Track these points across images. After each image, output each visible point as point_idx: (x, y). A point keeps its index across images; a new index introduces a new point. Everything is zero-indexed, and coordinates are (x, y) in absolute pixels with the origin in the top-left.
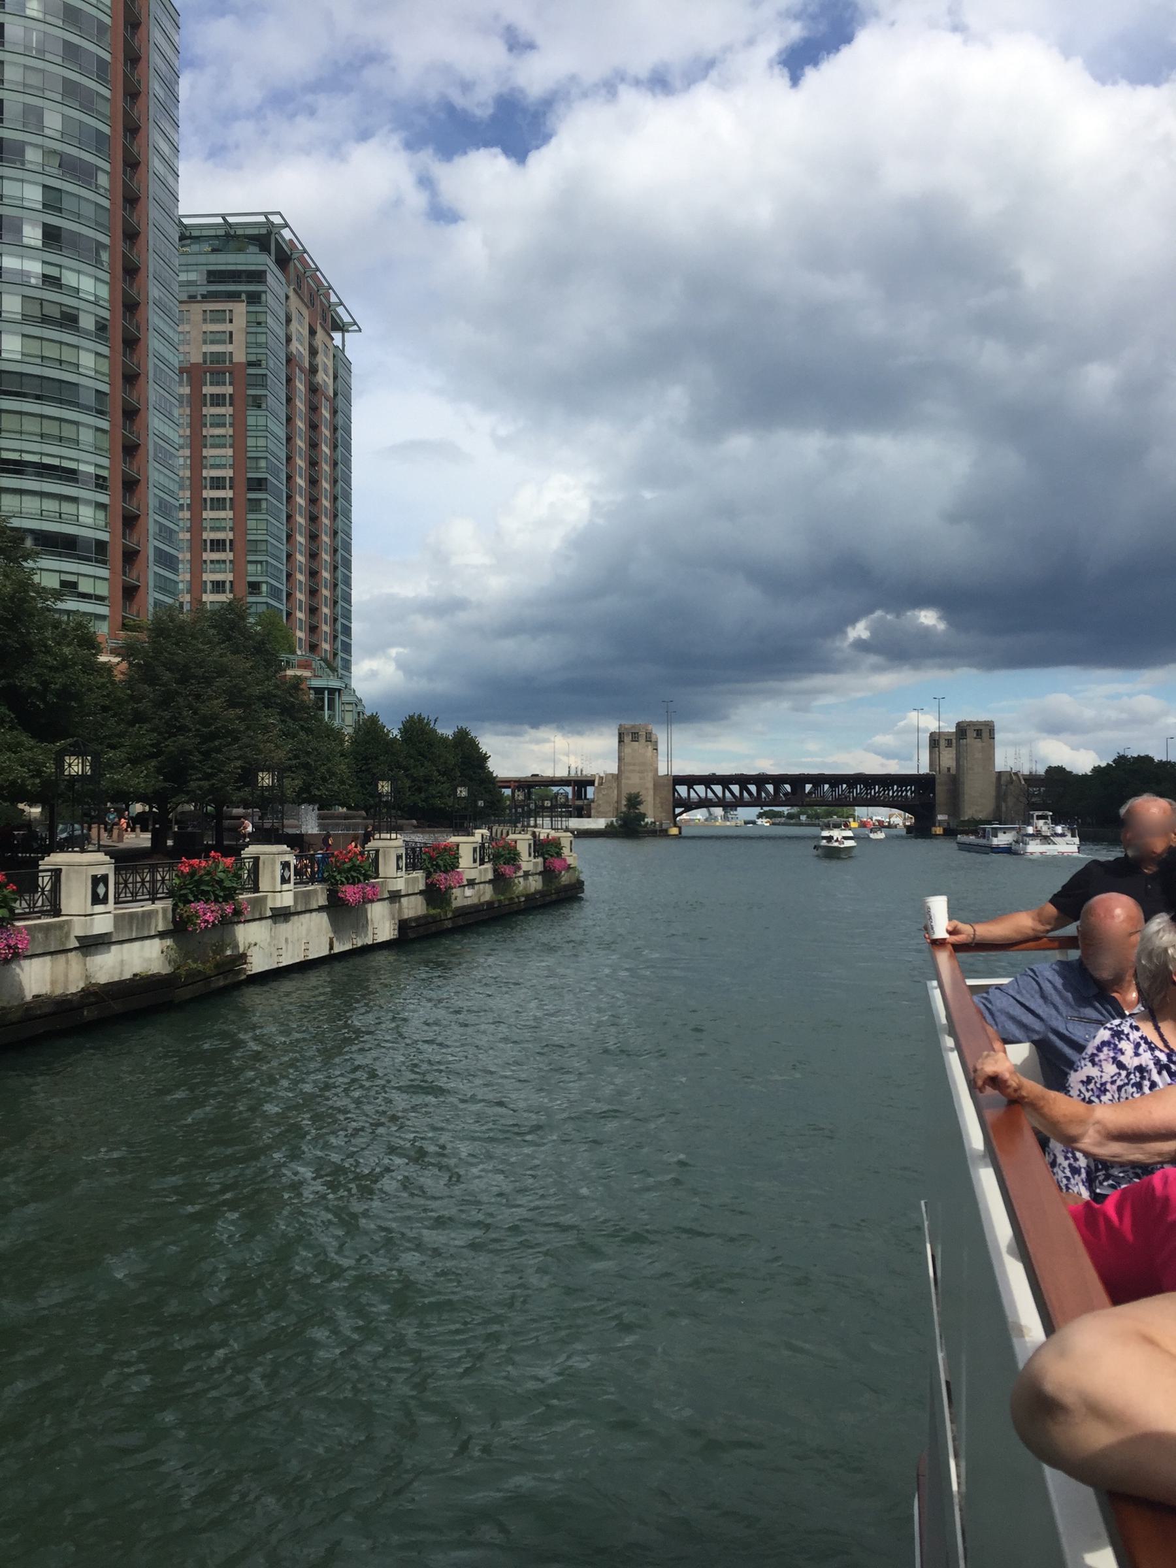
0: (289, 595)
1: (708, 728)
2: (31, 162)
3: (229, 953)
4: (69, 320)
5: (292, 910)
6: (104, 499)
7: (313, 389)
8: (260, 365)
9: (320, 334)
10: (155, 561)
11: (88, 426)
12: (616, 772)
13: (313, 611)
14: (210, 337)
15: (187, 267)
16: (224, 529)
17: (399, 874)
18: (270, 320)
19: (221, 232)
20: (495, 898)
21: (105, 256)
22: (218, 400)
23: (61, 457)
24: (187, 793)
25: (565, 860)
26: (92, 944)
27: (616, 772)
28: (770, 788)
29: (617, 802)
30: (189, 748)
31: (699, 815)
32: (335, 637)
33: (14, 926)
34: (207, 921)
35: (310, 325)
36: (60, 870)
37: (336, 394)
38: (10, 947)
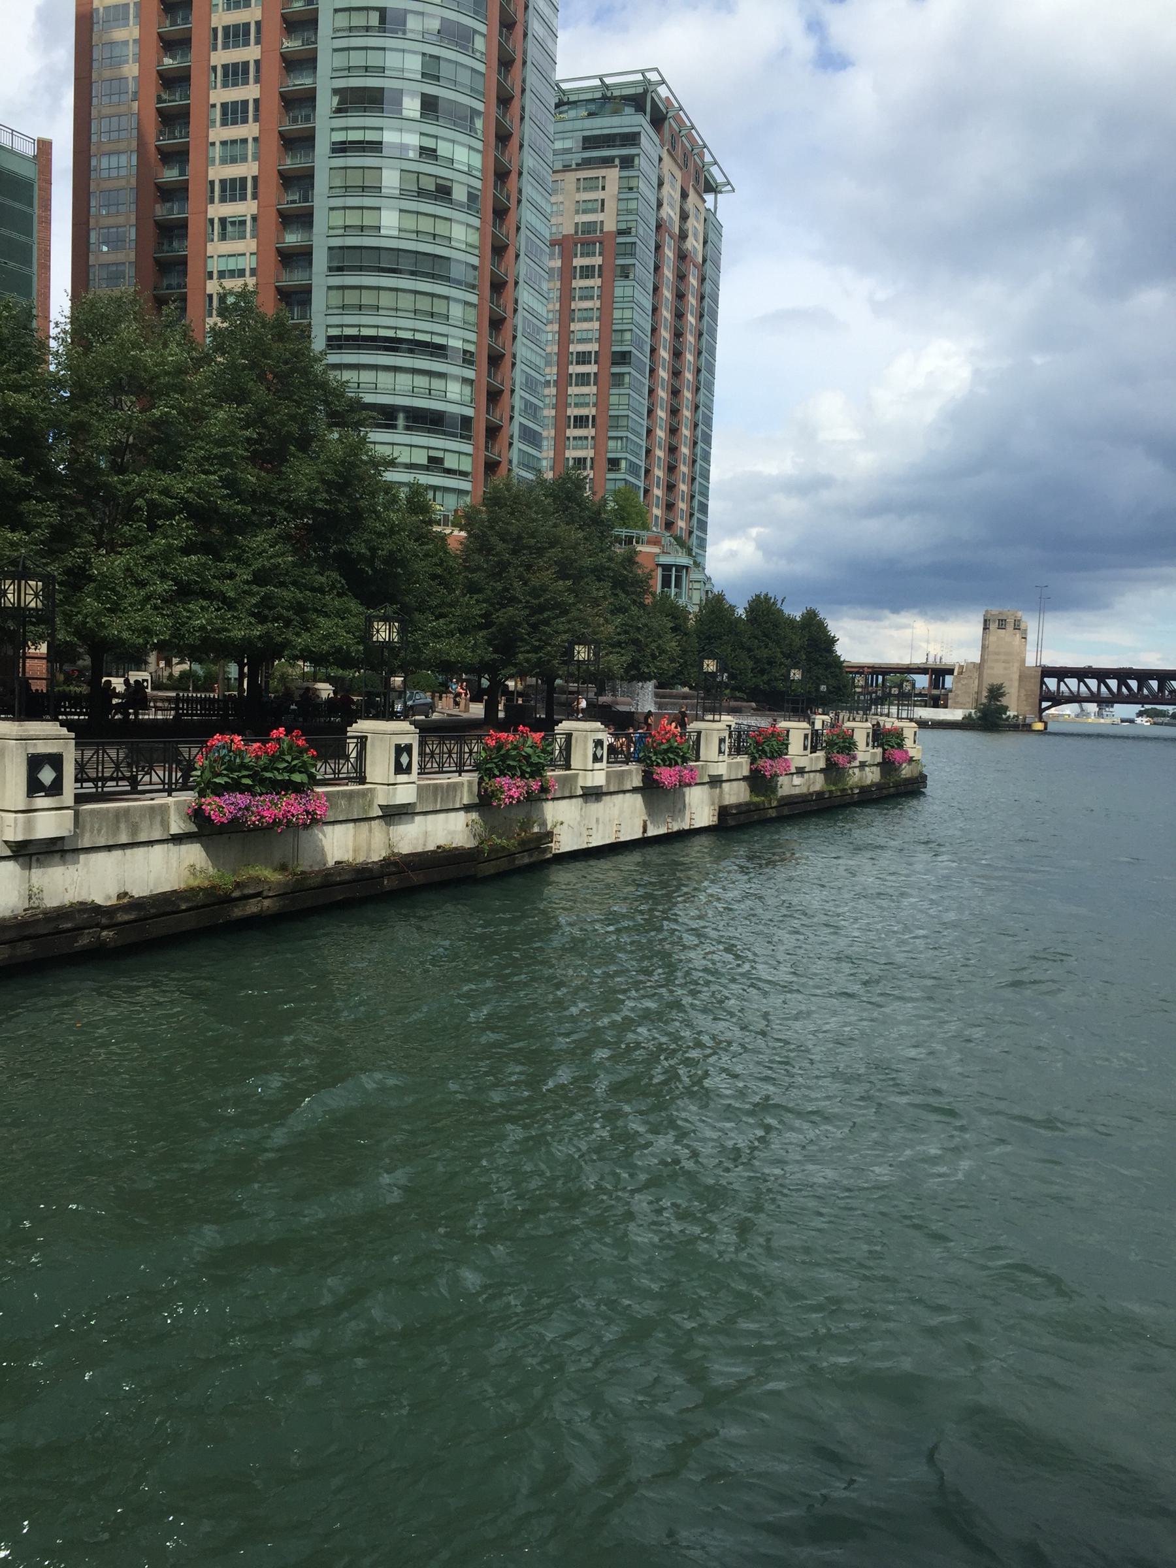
0: (647, 471)
1: (1087, 617)
2: (412, 31)
3: (536, 829)
4: (443, 192)
5: (605, 790)
6: (470, 374)
7: (682, 256)
8: (630, 233)
9: (692, 196)
12: (978, 660)
13: (671, 487)
14: (583, 206)
15: (563, 134)
16: (587, 405)
17: (721, 758)
18: (641, 185)
19: (598, 95)
20: (826, 788)
21: (479, 124)
22: (587, 272)
24: (515, 665)
25: (907, 752)
26: (395, 814)
27: (978, 660)
28: (1154, 684)
29: (977, 693)
30: (518, 620)
31: (1069, 710)
32: (692, 515)
33: (312, 790)
34: (512, 797)
36: (366, 737)
37: (704, 261)
38: (308, 813)
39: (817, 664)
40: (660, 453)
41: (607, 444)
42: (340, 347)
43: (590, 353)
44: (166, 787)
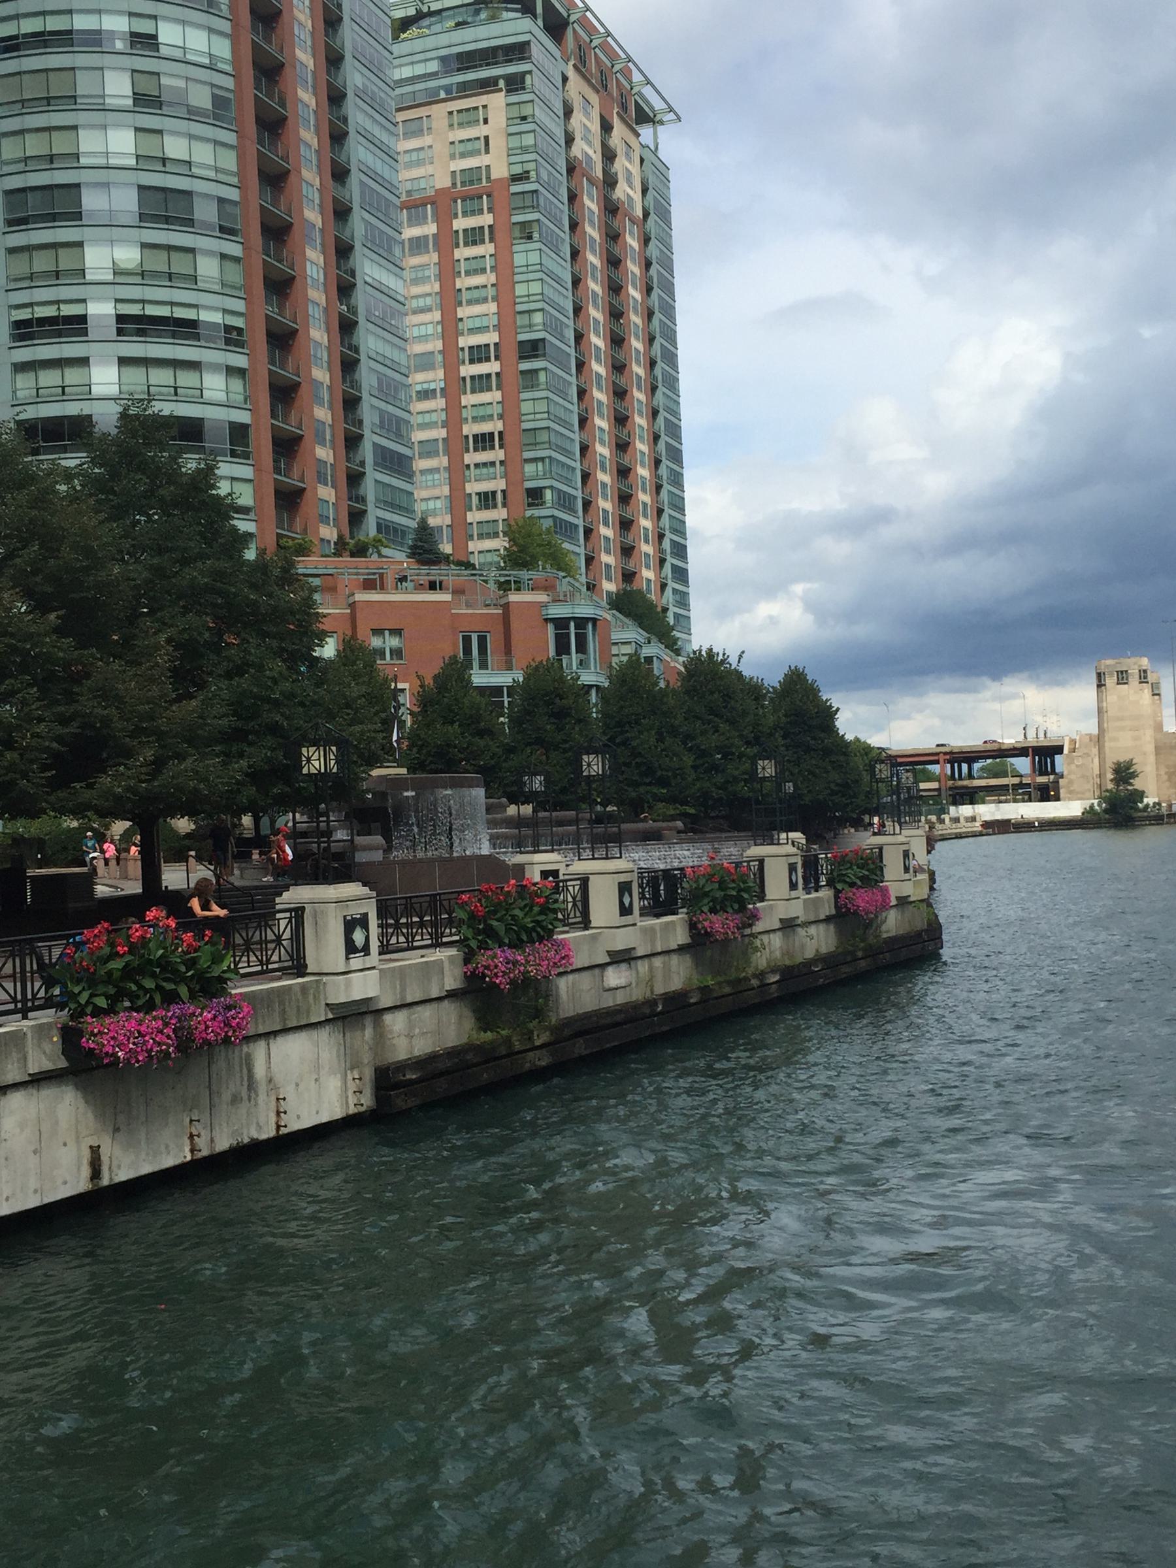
0: (587, 504)
7: (611, 209)
8: (528, 178)
9: (619, 129)
10: (376, 464)
11: (209, 253)
12: (1095, 731)
14: (460, 148)
16: (490, 417)
17: (794, 894)
22: (474, 236)
23: (172, 304)
32: (662, 561)
35: (602, 117)
37: (646, 214)
39: (808, 750)
40: (604, 477)
41: (523, 468)
43: (487, 345)
44: (19, 1005)
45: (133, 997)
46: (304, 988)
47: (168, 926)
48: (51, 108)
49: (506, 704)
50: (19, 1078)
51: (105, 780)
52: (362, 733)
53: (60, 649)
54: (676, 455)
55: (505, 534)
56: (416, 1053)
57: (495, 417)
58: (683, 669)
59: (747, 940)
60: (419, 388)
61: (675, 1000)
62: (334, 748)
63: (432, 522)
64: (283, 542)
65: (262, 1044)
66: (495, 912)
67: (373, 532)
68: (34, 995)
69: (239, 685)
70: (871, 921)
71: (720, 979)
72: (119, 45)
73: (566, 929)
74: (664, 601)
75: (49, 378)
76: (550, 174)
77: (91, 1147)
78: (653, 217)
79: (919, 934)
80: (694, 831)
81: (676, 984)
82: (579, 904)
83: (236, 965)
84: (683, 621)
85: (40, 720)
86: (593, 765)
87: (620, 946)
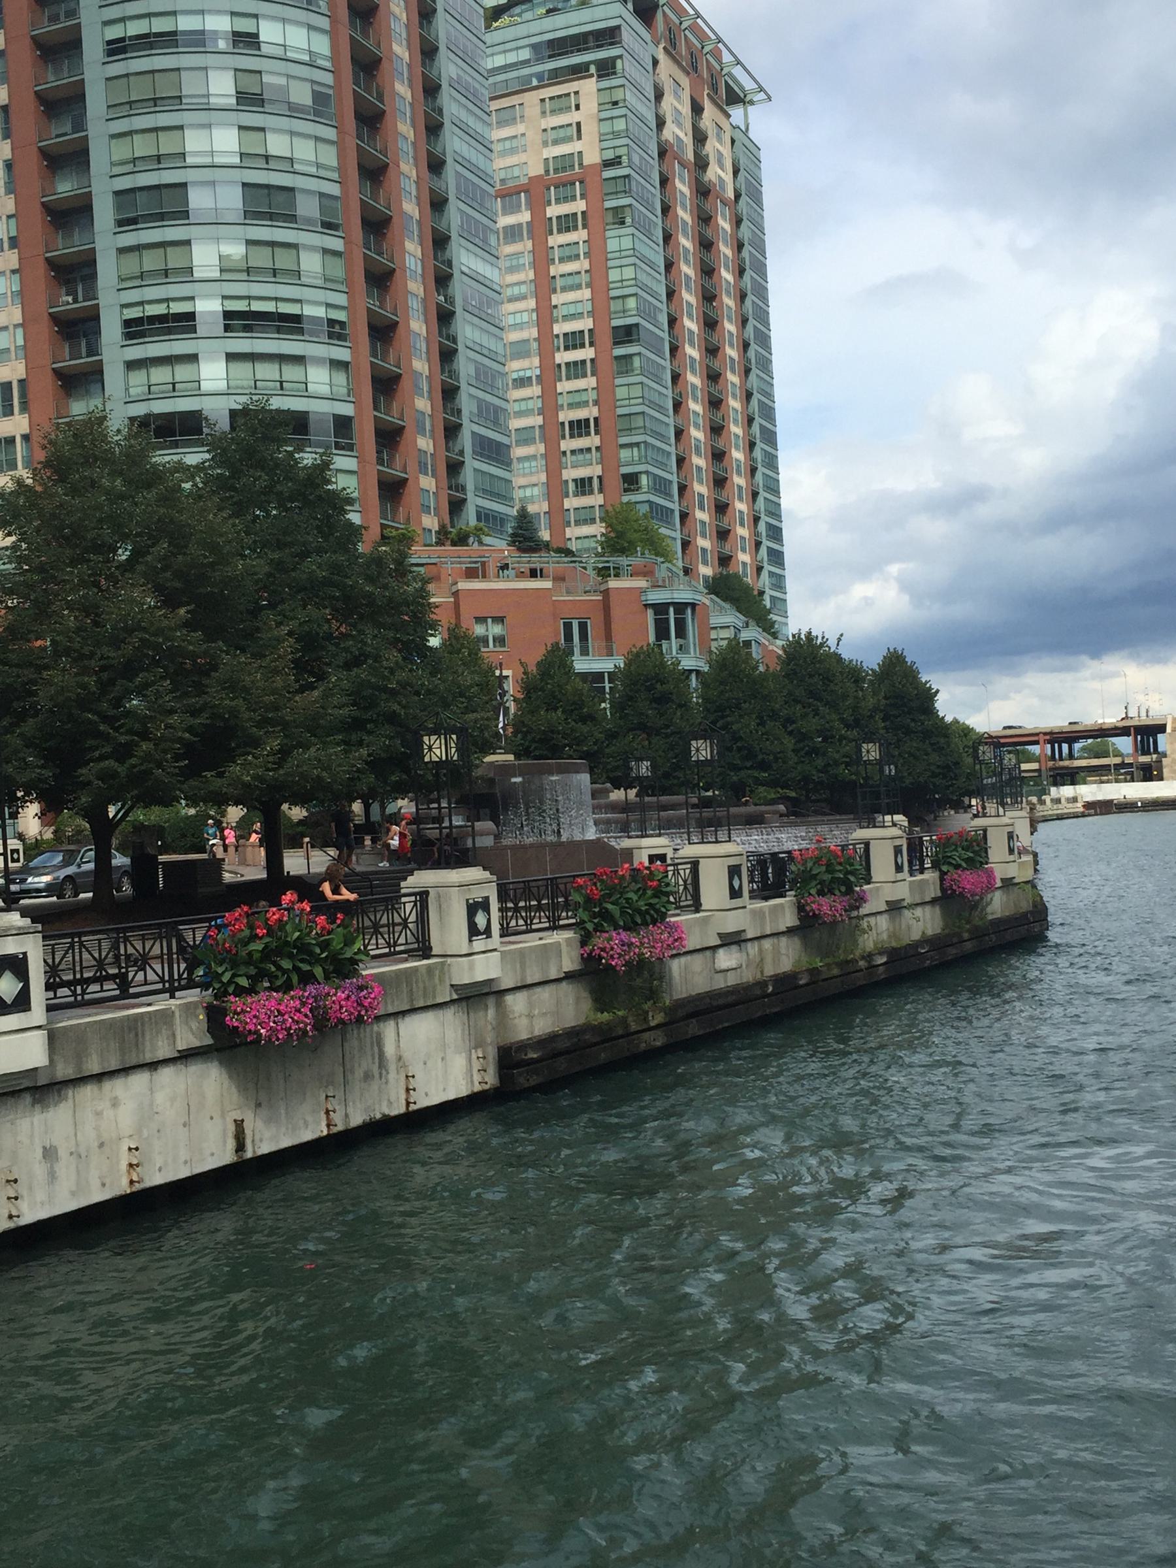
0: (682, 489)
6: (342, 353)
7: (703, 191)
8: (620, 163)
9: (709, 110)
10: (474, 452)
11: (312, 248)
14: (552, 135)
16: (585, 404)
17: (900, 876)
22: (567, 223)
32: (758, 544)
35: (692, 99)
36: (427, 893)
37: (738, 196)
39: (908, 732)
40: (699, 461)
42: (141, 334)
44: (167, 985)
45: (272, 978)
46: (429, 969)
47: (303, 910)
48: (157, 109)
49: (607, 690)
50: (169, 1055)
51: (235, 769)
52: (476, 721)
53: (190, 643)
54: (770, 438)
55: (602, 520)
56: (537, 1032)
57: (591, 403)
58: (780, 652)
59: (854, 922)
60: (515, 376)
61: (784, 981)
62: (454, 737)
63: (532, 509)
64: (387, 532)
65: (391, 1024)
66: (610, 896)
67: (473, 522)
68: (180, 976)
69: (358, 676)
70: (978, 901)
71: (828, 960)
72: (222, 45)
73: (678, 911)
74: (760, 584)
75: (160, 375)
76: (641, 158)
77: (235, 1121)
78: (744, 199)
79: (1024, 915)
80: (795, 814)
81: (786, 965)
82: (690, 887)
83: (365, 946)
84: (780, 603)
85: (172, 712)
86: (702, 750)
87: (731, 928)
